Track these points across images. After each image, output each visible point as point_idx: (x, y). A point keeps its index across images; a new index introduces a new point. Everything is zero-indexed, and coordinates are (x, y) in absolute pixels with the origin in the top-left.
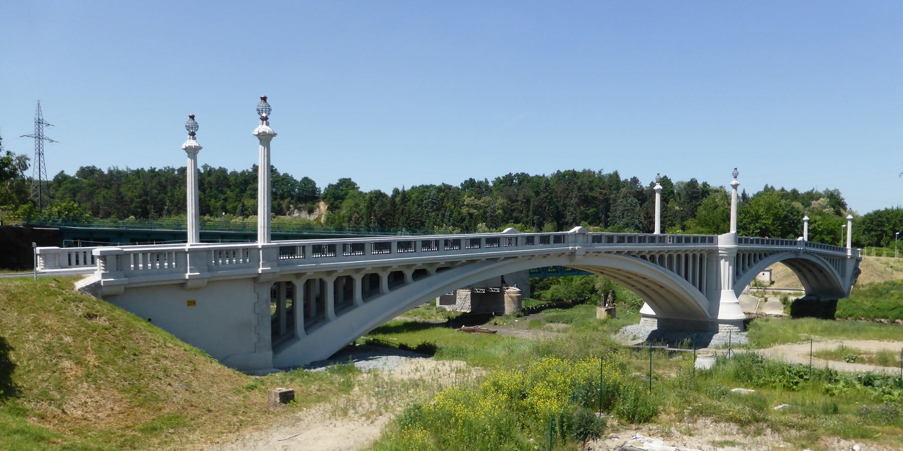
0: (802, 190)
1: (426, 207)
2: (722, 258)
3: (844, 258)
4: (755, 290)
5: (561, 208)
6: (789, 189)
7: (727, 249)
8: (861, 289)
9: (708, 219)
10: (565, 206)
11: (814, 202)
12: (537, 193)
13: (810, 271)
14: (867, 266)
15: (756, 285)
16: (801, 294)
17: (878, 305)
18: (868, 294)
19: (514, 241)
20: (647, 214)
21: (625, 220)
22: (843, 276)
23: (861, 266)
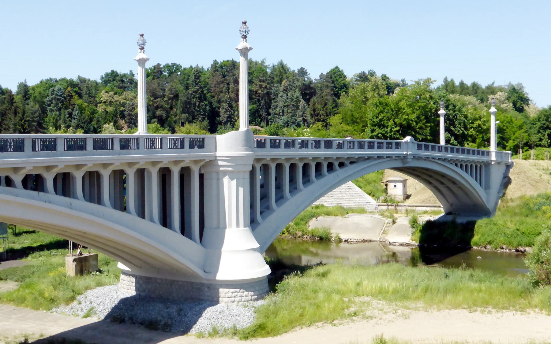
0: (484, 84)
1: (49, 105)
2: (225, 173)
3: (488, 164)
4: (385, 208)
5: (215, 105)
6: (468, 82)
7: (231, 159)
8: (510, 204)
9: (355, 114)
10: (219, 102)
11: (491, 96)
12: (187, 87)
13: (442, 183)
14: (519, 173)
15: (386, 201)
16: (439, 213)
17: (523, 228)
18: (517, 211)
19: (352, 144)
20: (314, 110)
21: (285, 118)
22: (487, 187)
23: (512, 175)
